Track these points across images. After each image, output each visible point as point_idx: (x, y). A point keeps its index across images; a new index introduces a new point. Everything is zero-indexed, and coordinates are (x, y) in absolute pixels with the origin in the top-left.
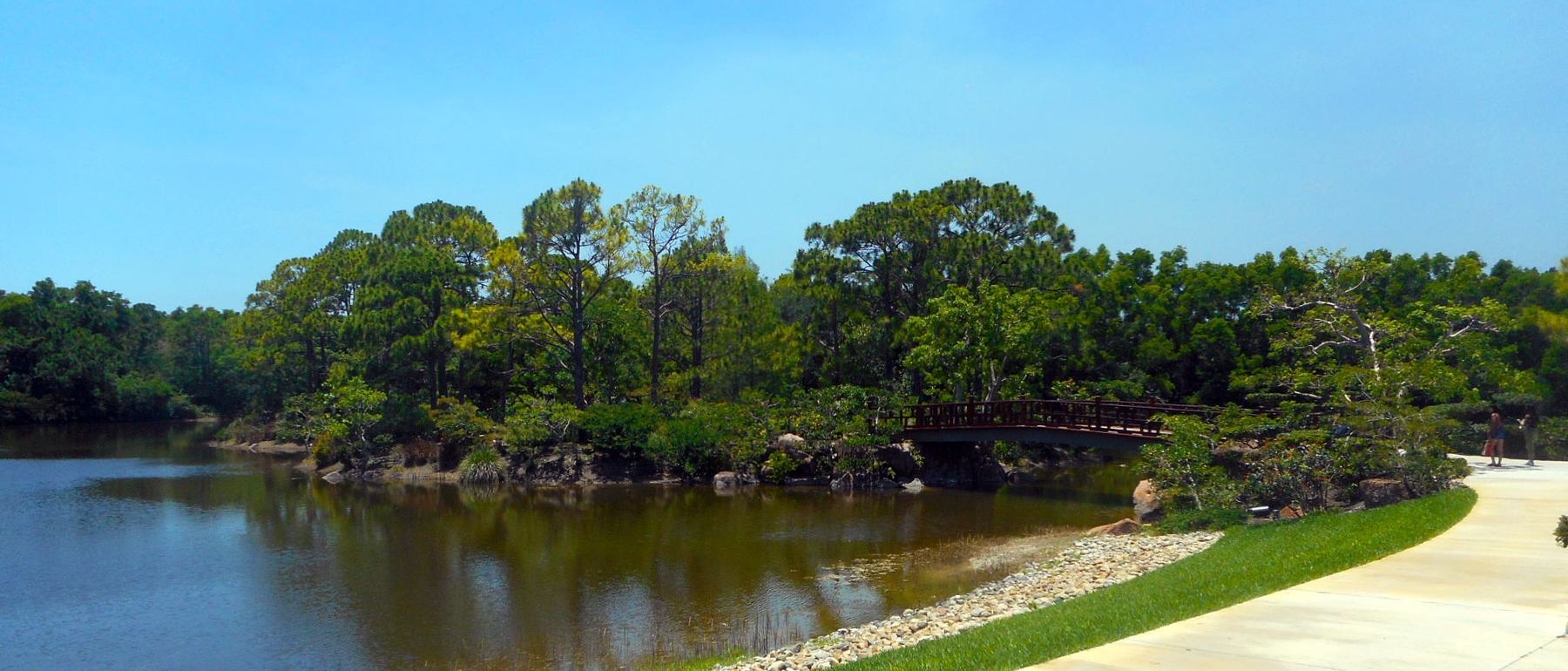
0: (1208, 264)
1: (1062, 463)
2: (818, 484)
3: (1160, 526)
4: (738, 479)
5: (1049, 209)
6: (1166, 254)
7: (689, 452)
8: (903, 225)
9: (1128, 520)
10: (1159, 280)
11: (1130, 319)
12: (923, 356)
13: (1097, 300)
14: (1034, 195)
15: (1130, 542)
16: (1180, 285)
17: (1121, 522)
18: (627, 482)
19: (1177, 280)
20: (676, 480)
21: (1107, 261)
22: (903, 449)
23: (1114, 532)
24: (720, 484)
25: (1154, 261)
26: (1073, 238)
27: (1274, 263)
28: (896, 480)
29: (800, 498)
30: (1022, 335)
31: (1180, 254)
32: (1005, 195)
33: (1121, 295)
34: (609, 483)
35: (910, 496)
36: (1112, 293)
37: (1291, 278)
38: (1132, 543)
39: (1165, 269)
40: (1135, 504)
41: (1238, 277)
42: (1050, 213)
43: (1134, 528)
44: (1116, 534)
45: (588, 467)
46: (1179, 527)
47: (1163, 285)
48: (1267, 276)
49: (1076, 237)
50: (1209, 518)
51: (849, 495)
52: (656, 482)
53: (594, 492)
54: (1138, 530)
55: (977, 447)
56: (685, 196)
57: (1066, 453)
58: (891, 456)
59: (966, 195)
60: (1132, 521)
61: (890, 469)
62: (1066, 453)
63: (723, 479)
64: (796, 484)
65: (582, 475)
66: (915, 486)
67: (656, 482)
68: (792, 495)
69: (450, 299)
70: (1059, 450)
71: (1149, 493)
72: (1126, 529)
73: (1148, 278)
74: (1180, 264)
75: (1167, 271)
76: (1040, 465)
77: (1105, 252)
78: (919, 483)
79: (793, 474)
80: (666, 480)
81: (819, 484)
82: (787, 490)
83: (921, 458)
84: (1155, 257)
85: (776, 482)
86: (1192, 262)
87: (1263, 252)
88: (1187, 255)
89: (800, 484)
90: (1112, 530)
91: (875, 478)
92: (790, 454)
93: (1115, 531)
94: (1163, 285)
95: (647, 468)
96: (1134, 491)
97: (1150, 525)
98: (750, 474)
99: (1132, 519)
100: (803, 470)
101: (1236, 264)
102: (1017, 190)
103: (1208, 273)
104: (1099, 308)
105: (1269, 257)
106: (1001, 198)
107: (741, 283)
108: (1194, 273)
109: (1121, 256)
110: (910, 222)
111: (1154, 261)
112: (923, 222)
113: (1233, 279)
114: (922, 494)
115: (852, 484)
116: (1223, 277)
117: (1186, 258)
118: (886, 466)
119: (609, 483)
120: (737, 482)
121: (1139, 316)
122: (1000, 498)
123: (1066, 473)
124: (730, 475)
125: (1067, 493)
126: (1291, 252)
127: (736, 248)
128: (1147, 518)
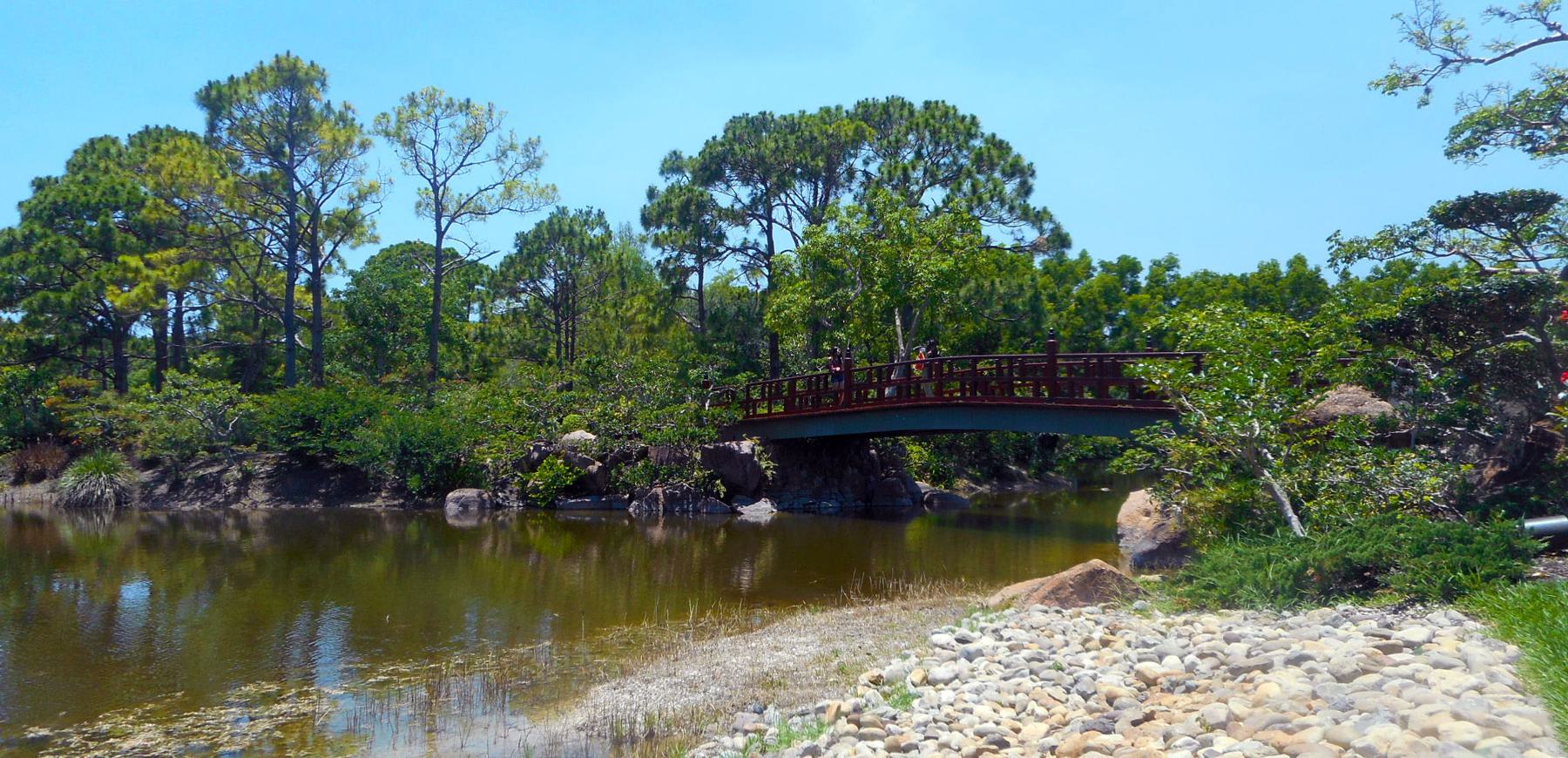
0: (1206, 273)
1: (1017, 487)
2: (609, 507)
3: (1189, 580)
4: (484, 501)
5: (999, 137)
6: (1156, 263)
7: (407, 457)
8: (786, 141)
9: (1096, 563)
10: (1148, 290)
11: (1116, 333)
12: (789, 308)
13: (1077, 309)
14: (980, 119)
15: (1098, 633)
16: (1173, 298)
17: (1079, 569)
18: (315, 505)
19: (1169, 292)
20: (396, 502)
21: (1089, 267)
22: (740, 448)
23: (1060, 598)
24: (451, 508)
25: (1142, 269)
26: (1033, 174)
27: (1280, 273)
28: (728, 498)
29: (582, 533)
30: (941, 272)
31: (1172, 263)
32: (937, 114)
33: (1106, 303)
34: (286, 506)
35: (756, 527)
36: (1094, 300)
37: (1301, 288)
38: (1105, 643)
39: (1155, 280)
40: (1122, 536)
41: (1241, 287)
42: (1001, 142)
43: (1115, 587)
44: (1064, 603)
45: (261, 482)
46: (1256, 584)
47: (1153, 297)
48: (1273, 287)
49: (1037, 173)
50: (1379, 554)
51: (657, 524)
52: (360, 506)
53: (267, 521)
54: (1130, 594)
55: (873, 451)
56: (479, 103)
57: (1024, 472)
58: (720, 460)
59: (885, 117)
60: (1109, 567)
61: (718, 482)
62: (1024, 472)
63: (457, 500)
64: (571, 508)
65: (247, 495)
66: (761, 511)
67: (360, 506)
68: (568, 526)
69: (123, 243)
70: (1014, 468)
71: (1148, 514)
72: (1091, 590)
73: (1135, 289)
74: (1172, 273)
75: (1157, 282)
76: (985, 489)
77: (1087, 257)
78: (769, 505)
79: (570, 491)
80: (379, 504)
81: (611, 509)
82: (561, 516)
83: (772, 464)
84: (1143, 265)
85: (542, 505)
86: (1185, 271)
87: (1267, 260)
88: (1180, 263)
89: (579, 509)
90: (1053, 592)
91: (696, 498)
92: (567, 461)
93: (1063, 594)
94: (1153, 297)
95: (357, 482)
96: (1117, 510)
97: (1156, 577)
98: (511, 492)
99: (1116, 565)
100: (582, 486)
101: (1238, 274)
102: (956, 111)
103: (1205, 282)
104: (1079, 318)
105: (1275, 265)
106: (933, 117)
107: (617, 262)
108: (1189, 283)
109: (1103, 265)
110: (798, 138)
111: (1142, 269)
112: (816, 138)
113: (1235, 289)
114: (774, 526)
115: (661, 507)
116: (1223, 288)
117: (1178, 267)
118: (712, 477)
119: (286, 506)
120: (482, 505)
121: (1126, 329)
122: (914, 531)
123: (1025, 500)
124: (470, 493)
125: (1029, 525)
126: (1299, 260)
127: (620, 225)
128: (1145, 562)
